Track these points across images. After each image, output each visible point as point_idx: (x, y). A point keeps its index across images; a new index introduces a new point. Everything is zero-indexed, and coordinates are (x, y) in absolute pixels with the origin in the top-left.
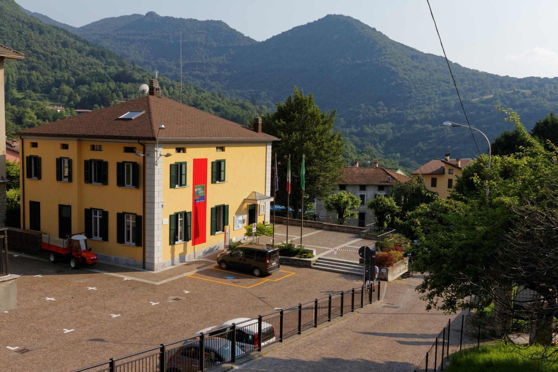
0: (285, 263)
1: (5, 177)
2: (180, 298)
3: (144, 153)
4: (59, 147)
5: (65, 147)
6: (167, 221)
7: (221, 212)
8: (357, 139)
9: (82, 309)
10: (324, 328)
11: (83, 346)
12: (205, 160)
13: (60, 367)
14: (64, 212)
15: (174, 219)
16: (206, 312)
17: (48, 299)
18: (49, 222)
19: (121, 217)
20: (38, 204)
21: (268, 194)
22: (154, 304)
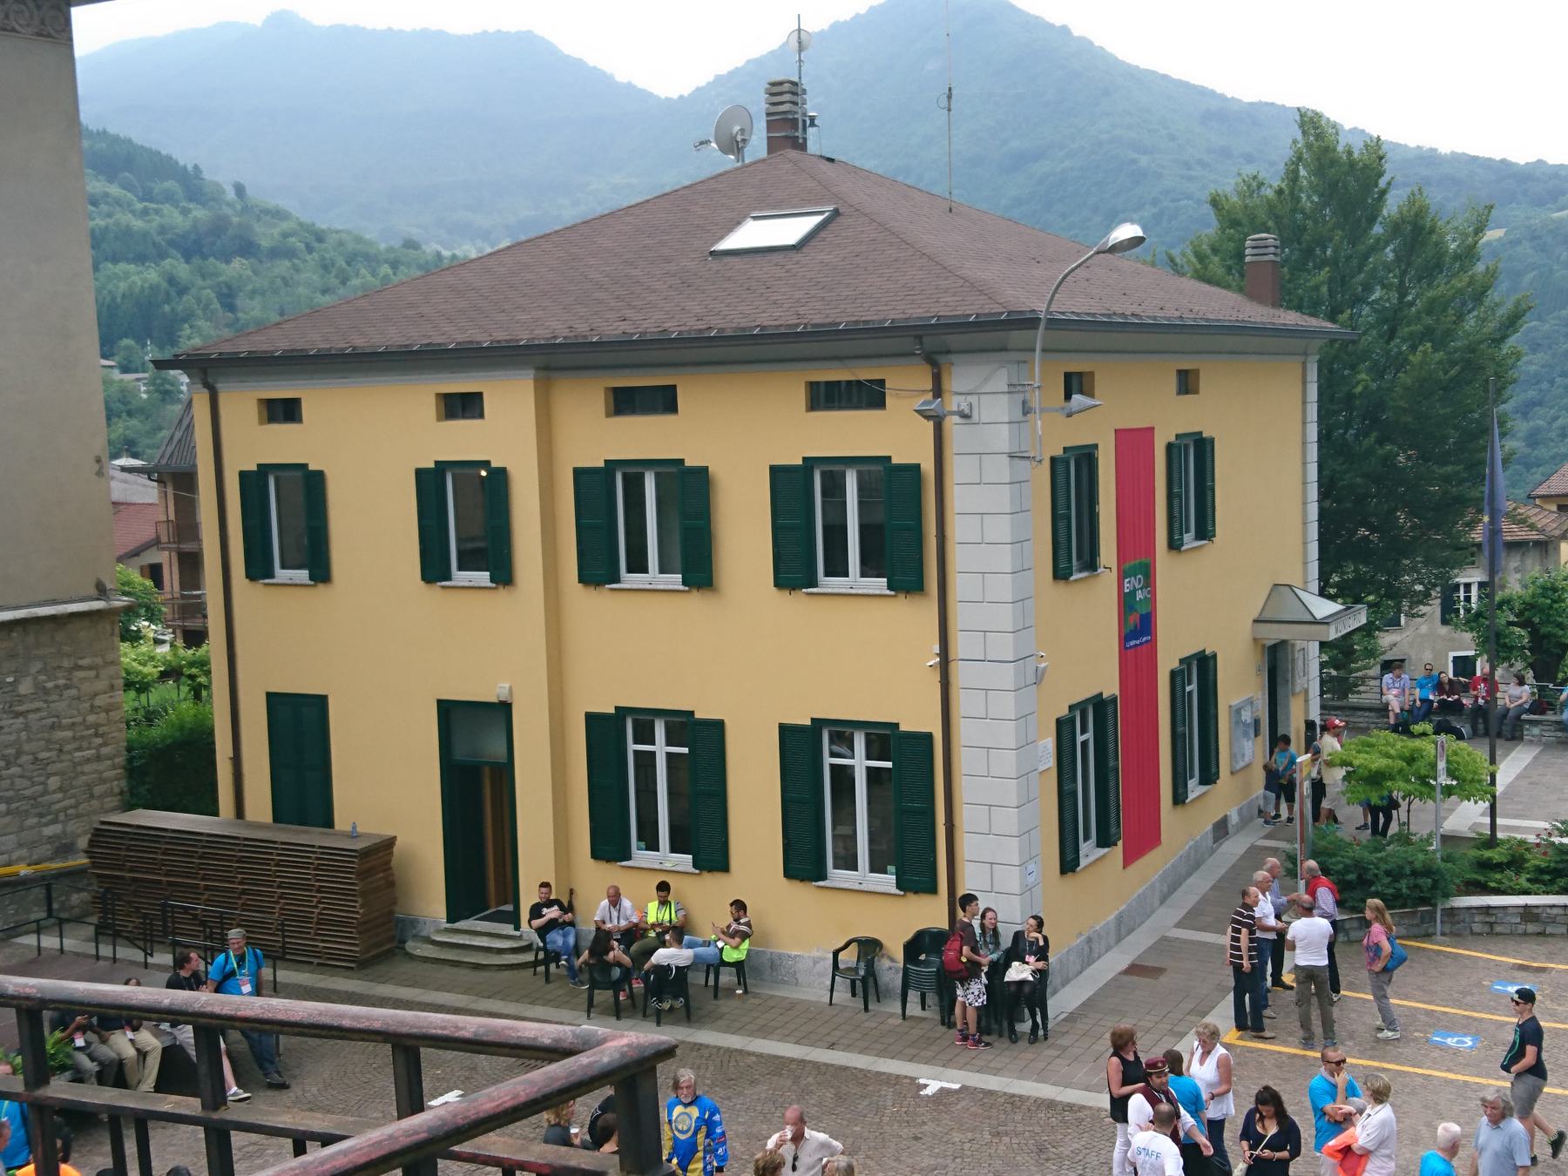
4: (430, 407)
5: (463, 406)
18: (389, 792)
19: (800, 746)
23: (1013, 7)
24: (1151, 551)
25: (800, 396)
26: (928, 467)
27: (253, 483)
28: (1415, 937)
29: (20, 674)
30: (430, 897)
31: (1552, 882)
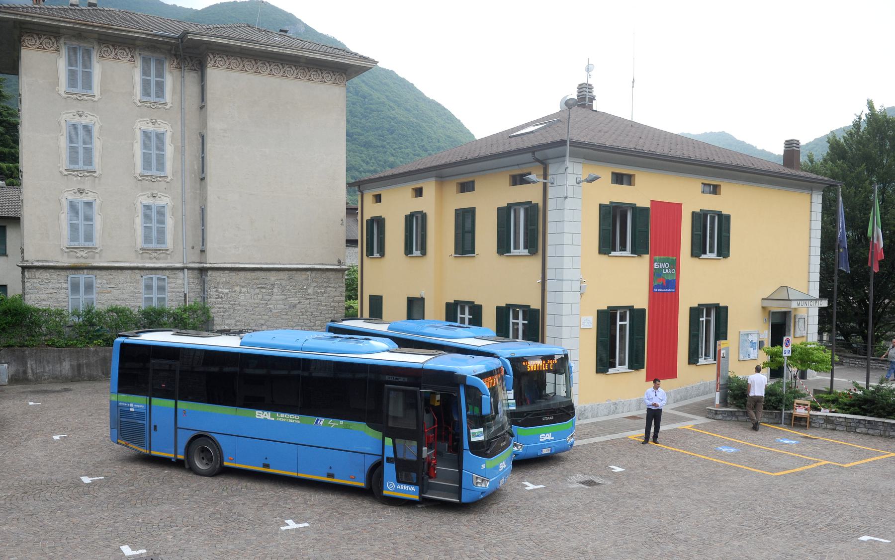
0: (864, 430)
2: (597, 481)
3: (545, 177)
6: (590, 322)
7: (713, 321)
12: (678, 207)
15: (606, 319)
16: (654, 521)
20: (380, 298)
23: (163, 3)
24: (677, 252)
25: (507, 180)
26: (541, 205)
28: (771, 424)
29: (308, 286)
31: (849, 409)
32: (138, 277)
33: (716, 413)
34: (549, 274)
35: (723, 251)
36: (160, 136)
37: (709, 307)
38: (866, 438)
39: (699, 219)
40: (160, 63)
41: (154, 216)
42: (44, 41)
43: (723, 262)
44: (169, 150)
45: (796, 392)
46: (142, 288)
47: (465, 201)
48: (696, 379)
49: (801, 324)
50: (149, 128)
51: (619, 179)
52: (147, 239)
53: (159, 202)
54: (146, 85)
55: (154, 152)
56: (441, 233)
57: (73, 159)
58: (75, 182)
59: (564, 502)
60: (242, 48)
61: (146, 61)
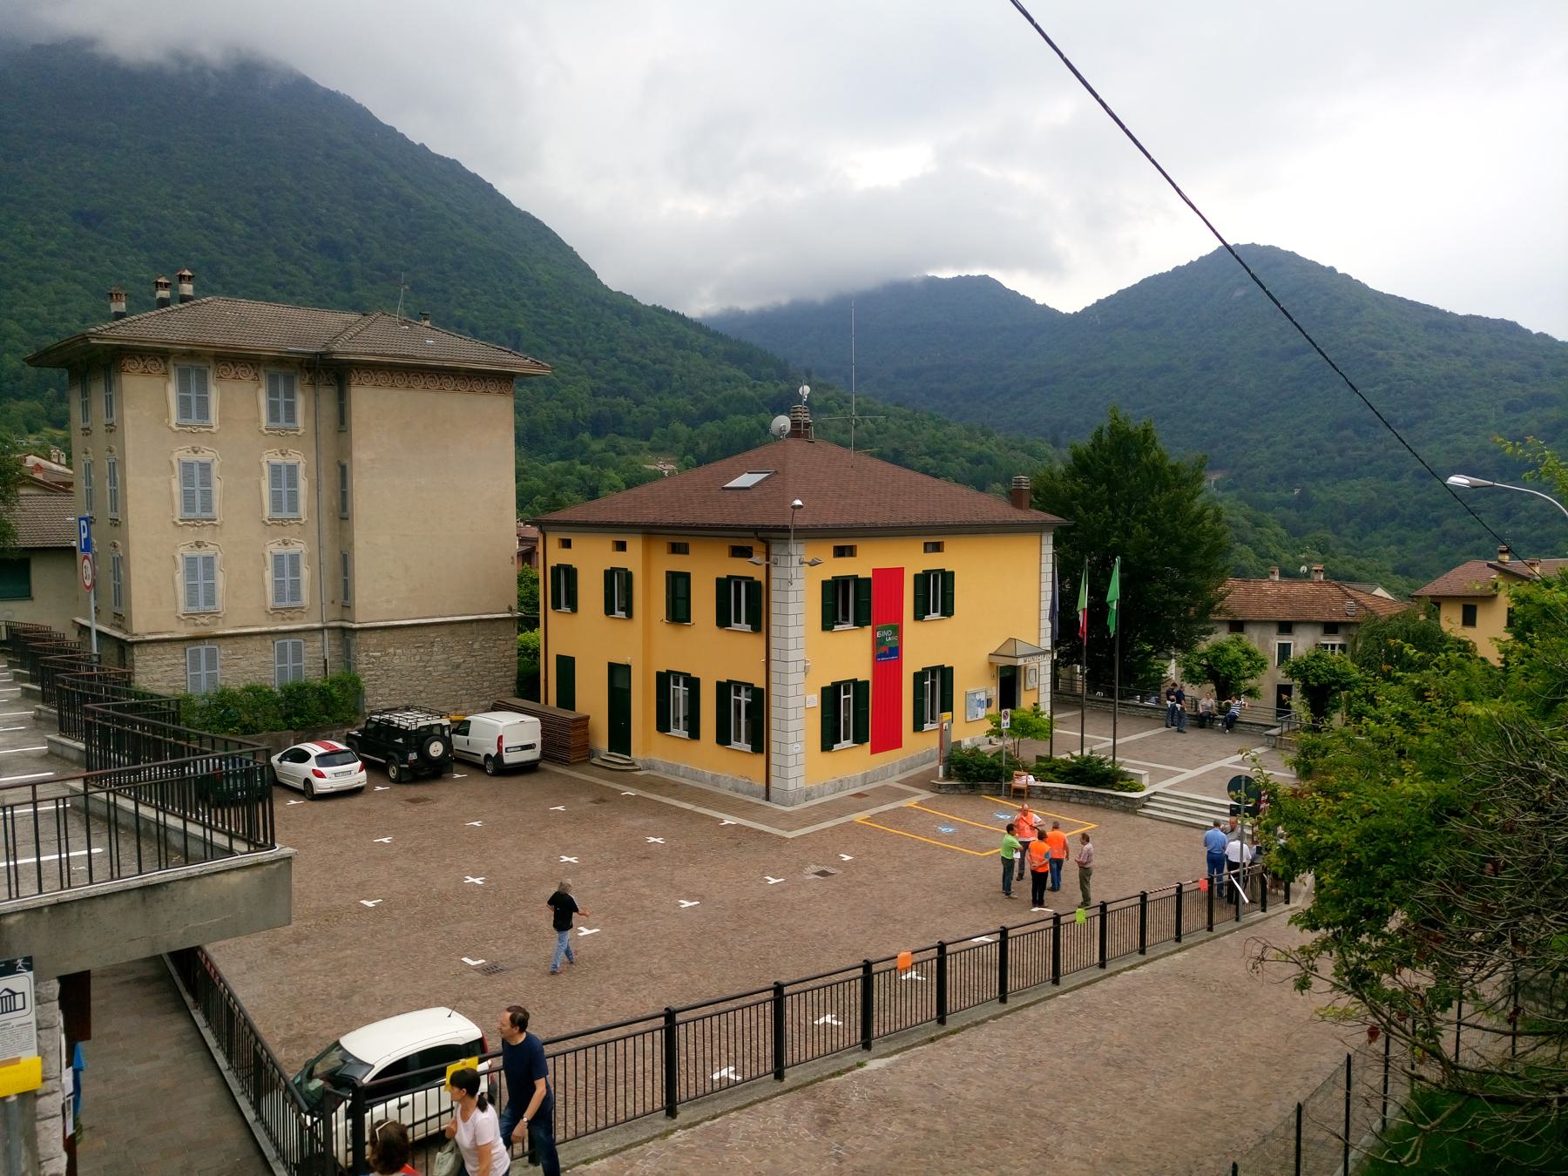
1: (515, 607)
5: (621, 546)
6: (815, 700)
8: (1292, 515)
9: (625, 884)
10: (1132, 977)
11: (608, 968)
12: (899, 572)
13: (553, 1012)
14: (619, 675)
15: (831, 695)
17: (566, 859)
19: (724, 689)
21: (1046, 643)
22: (773, 881)
25: (727, 551)
27: (556, 570)
30: (602, 741)
32: (269, 643)
33: (940, 786)
34: (774, 655)
35: (948, 611)
36: (292, 469)
37: (933, 670)
38: (1077, 807)
39: (922, 580)
40: (289, 381)
41: (286, 566)
42: (149, 363)
43: (948, 621)
44: (303, 486)
45: (1017, 763)
46: (273, 656)
47: (678, 564)
48: (920, 747)
49: (1032, 675)
50: (279, 460)
51: (840, 552)
52: (279, 596)
53: (292, 550)
54: (273, 407)
55: (285, 489)
56: (651, 596)
57: (189, 505)
58: (191, 535)
59: (804, 894)
60: (390, 364)
61: (273, 380)
